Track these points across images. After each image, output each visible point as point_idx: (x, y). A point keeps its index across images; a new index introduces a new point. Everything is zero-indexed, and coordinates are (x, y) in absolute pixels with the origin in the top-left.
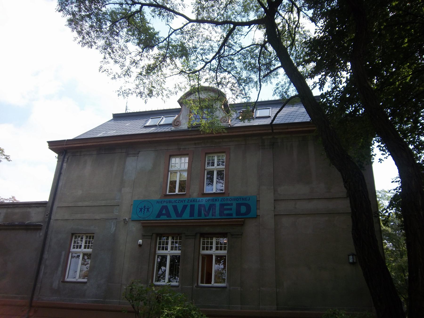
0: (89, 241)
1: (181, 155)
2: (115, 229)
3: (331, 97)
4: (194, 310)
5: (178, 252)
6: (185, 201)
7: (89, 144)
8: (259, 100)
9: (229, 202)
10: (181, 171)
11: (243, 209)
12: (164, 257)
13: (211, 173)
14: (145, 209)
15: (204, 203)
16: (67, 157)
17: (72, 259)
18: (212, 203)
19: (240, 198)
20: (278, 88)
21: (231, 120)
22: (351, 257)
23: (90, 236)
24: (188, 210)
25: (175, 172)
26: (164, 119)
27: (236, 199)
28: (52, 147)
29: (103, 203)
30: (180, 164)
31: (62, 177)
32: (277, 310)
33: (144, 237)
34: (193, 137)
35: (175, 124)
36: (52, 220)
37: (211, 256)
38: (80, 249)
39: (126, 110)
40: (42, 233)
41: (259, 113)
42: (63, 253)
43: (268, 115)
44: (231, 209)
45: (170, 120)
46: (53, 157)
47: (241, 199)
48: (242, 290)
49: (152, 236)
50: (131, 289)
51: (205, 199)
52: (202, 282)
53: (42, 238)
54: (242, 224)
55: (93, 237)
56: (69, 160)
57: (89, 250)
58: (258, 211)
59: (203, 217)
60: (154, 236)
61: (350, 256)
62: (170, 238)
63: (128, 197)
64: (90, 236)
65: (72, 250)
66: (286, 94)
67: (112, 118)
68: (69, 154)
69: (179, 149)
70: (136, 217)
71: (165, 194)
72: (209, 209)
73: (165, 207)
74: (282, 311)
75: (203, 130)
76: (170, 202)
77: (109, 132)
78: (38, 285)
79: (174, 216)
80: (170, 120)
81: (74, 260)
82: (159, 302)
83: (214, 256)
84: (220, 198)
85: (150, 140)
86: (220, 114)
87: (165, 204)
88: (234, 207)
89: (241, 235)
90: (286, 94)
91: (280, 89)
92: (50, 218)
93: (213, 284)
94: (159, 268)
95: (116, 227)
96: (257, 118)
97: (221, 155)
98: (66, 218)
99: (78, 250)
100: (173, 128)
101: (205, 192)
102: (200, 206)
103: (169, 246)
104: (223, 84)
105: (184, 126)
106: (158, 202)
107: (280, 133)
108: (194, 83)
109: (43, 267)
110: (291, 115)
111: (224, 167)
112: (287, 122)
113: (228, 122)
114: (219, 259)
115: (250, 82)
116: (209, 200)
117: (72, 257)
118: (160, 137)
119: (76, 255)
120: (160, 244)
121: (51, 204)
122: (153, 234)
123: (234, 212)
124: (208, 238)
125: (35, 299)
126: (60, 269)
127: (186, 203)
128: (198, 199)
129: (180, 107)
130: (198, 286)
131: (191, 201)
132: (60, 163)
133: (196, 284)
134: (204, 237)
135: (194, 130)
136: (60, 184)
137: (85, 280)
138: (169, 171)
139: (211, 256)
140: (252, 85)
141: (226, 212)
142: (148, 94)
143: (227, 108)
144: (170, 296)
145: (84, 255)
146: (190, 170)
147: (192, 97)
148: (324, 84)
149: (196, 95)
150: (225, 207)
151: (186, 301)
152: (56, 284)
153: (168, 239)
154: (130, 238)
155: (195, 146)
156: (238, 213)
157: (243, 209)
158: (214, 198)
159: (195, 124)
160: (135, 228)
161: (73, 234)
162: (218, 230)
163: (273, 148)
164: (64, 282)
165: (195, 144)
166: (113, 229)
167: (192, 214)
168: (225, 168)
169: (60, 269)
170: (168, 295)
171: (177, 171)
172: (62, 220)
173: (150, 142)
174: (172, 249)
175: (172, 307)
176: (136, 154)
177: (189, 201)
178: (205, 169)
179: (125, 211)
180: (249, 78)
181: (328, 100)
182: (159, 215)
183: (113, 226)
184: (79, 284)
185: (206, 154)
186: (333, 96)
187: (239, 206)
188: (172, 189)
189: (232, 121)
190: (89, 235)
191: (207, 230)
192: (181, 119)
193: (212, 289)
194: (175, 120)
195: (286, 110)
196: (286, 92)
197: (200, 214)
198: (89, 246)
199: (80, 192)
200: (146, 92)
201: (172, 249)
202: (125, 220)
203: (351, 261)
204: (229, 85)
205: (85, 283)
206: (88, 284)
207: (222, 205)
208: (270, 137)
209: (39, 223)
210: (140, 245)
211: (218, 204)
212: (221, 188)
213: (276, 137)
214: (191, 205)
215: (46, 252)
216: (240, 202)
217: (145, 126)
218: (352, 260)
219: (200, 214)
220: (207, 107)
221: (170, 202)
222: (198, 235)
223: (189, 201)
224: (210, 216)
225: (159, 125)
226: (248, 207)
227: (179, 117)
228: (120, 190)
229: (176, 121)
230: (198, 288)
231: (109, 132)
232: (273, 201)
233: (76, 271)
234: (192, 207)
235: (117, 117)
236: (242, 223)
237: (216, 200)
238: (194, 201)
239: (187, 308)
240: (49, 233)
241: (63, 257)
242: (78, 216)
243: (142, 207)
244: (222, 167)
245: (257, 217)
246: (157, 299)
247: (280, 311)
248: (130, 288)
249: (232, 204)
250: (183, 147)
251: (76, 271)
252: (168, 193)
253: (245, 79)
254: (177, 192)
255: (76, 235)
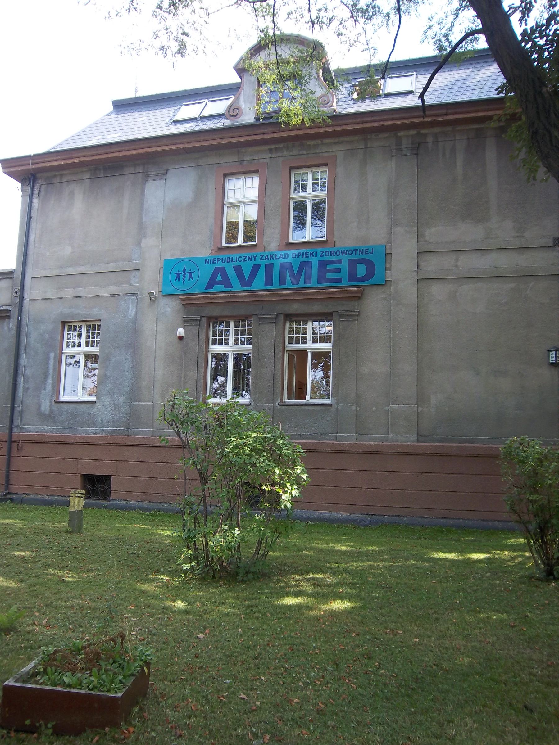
0: (93, 334)
1: (246, 172)
2: (136, 312)
3: (541, 38)
4: (282, 439)
5: (246, 348)
6: (255, 258)
7: (76, 160)
8: (392, 60)
9: (334, 258)
10: (246, 203)
11: (361, 270)
12: (221, 359)
13: (300, 207)
14: (185, 274)
15: (289, 260)
16: (37, 187)
17: (67, 368)
18: (304, 259)
19: (356, 250)
20: (430, 27)
21: (337, 102)
22: (552, 354)
23: (94, 327)
24: (262, 272)
25: (236, 206)
26: (210, 103)
27: (349, 252)
28: (7, 170)
29: (111, 267)
30: (244, 194)
31: (33, 224)
32: (418, 441)
33: (186, 323)
34: (266, 137)
35: (232, 114)
36: (25, 302)
37: (305, 353)
38: (78, 347)
39: (136, 91)
40: (12, 324)
41: (393, 84)
42: (52, 355)
43: (407, 88)
44: (338, 271)
45: (219, 106)
46: (14, 187)
47: (358, 252)
48: (358, 409)
49: (200, 321)
50: (173, 406)
51: (291, 252)
52: (289, 398)
53: (14, 332)
54: (359, 297)
55: (99, 326)
56: (43, 193)
57: (94, 350)
58: (388, 273)
59: (289, 285)
60: (204, 320)
61: (551, 353)
62: (232, 325)
63: (153, 255)
64: (94, 327)
65: (66, 349)
66: (447, 39)
67: (111, 108)
68: (40, 181)
69: (241, 162)
70: (170, 290)
71: (219, 246)
72: (300, 272)
73: (222, 271)
74: (426, 444)
75: (286, 120)
76: (229, 260)
77: (109, 136)
78: (18, 409)
79: (237, 285)
80: (219, 106)
81: (70, 369)
82: (221, 425)
83: (309, 353)
84: (319, 250)
85: (186, 146)
86: (317, 88)
87: (220, 264)
88: (345, 266)
89: (358, 315)
90: (447, 39)
91: (436, 28)
92: (22, 299)
93: (309, 399)
94: (214, 378)
95: (137, 308)
96: (387, 95)
97: (320, 169)
98: (49, 295)
99: (76, 349)
100: (227, 122)
101: (291, 241)
102: (282, 266)
103: (232, 337)
104: (322, 22)
105: (248, 117)
106: (207, 261)
107: (432, 124)
108: (266, 22)
109: (21, 380)
110: (454, 86)
111: (325, 193)
112: (446, 100)
113: (332, 106)
114: (320, 358)
115: (375, 14)
116: (299, 255)
117: (66, 364)
118: (204, 140)
119: (72, 361)
120: (214, 334)
121: (20, 274)
122: (201, 317)
123: (344, 274)
124: (298, 323)
125: (15, 431)
126: (50, 381)
127: (258, 262)
128: (279, 254)
129: (239, 80)
130: (282, 404)
131: (267, 258)
132: (27, 198)
133: (279, 401)
134: (291, 322)
135: (268, 123)
136: (32, 238)
137: (93, 399)
138: (223, 204)
139: (305, 353)
140: (378, 20)
141: (329, 276)
142: (179, 52)
143: (330, 79)
144: (240, 415)
145: (88, 358)
146: (262, 202)
147: (261, 59)
148: (529, 11)
149: (270, 50)
150: (328, 267)
151: (266, 423)
152: (45, 407)
153: (227, 326)
154: (161, 326)
155: (270, 155)
156: (352, 277)
157: (361, 270)
158: (308, 250)
159: (270, 108)
160: (170, 308)
161: (64, 323)
162: (316, 308)
163: (417, 154)
164: (58, 402)
165: (271, 150)
166: (132, 312)
167: (269, 280)
168: (328, 195)
169: (50, 381)
170: (236, 413)
171: (239, 203)
172: (43, 300)
173: (187, 151)
174: (236, 342)
175: (245, 434)
176: (163, 175)
177: (264, 258)
178: (290, 199)
179: (150, 280)
180: (374, 7)
181: (535, 44)
182: (210, 285)
183: (131, 306)
184: (83, 406)
185: (292, 169)
186: (547, 36)
187: (353, 264)
188: (232, 237)
189: (340, 103)
190: (91, 323)
191: (295, 308)
192: (241, 102)
193: (306, 407)
194: (230, 106)
195: (444, 78)
196: (446, 36)
197: (283, 281)
198: (93, 342)
199: (68, 250)
200: (175, 46)
201: (236, 342)
202: (151, 295)
203: (552, 360)
204: (335, 23)
205: (95, 402)
206: (98, 404)
207: (322, 265)
208: (413, 132)
209: (5, 308)
210: (181, 338)
211: (315, 261)
212: (320, 235)
213: (423, 131)
214: (267, 265)
215: (23, 356)
216: (353, 257)
217: (174, 122)
218: (554, 359)
219: (283, 281)
220: (293, 76)
221: (229, 260)
222: (282, 318)
223: (264, 258)
224: (301, 284)
225: (201, 118)
226: (369, 264)
227: (237, 99)
228: (139, 244)
229: (232, 108)
230: (284, 407)
231: (109, 136)
232: (415, 255)
233: (76, 385)
234: (269, 268)
235: (122, 106)
236: (360, 295)
237: (311, 254)
238: (271, 257)
239: (269, 435)
240: (24, 322)
241: (52, 362)
242: (70, 292)
243: (178, 271)
244: (322, 193)
245: (386, 283)
246: (217, 421)
247: (423, 444)
248: (171, 403)
249: (340, 262)
250: (248, 158)
251: (76, 385)
252: (224, 245)
253: (365, 8)
254: (240, 242)
255: (70, 324)
